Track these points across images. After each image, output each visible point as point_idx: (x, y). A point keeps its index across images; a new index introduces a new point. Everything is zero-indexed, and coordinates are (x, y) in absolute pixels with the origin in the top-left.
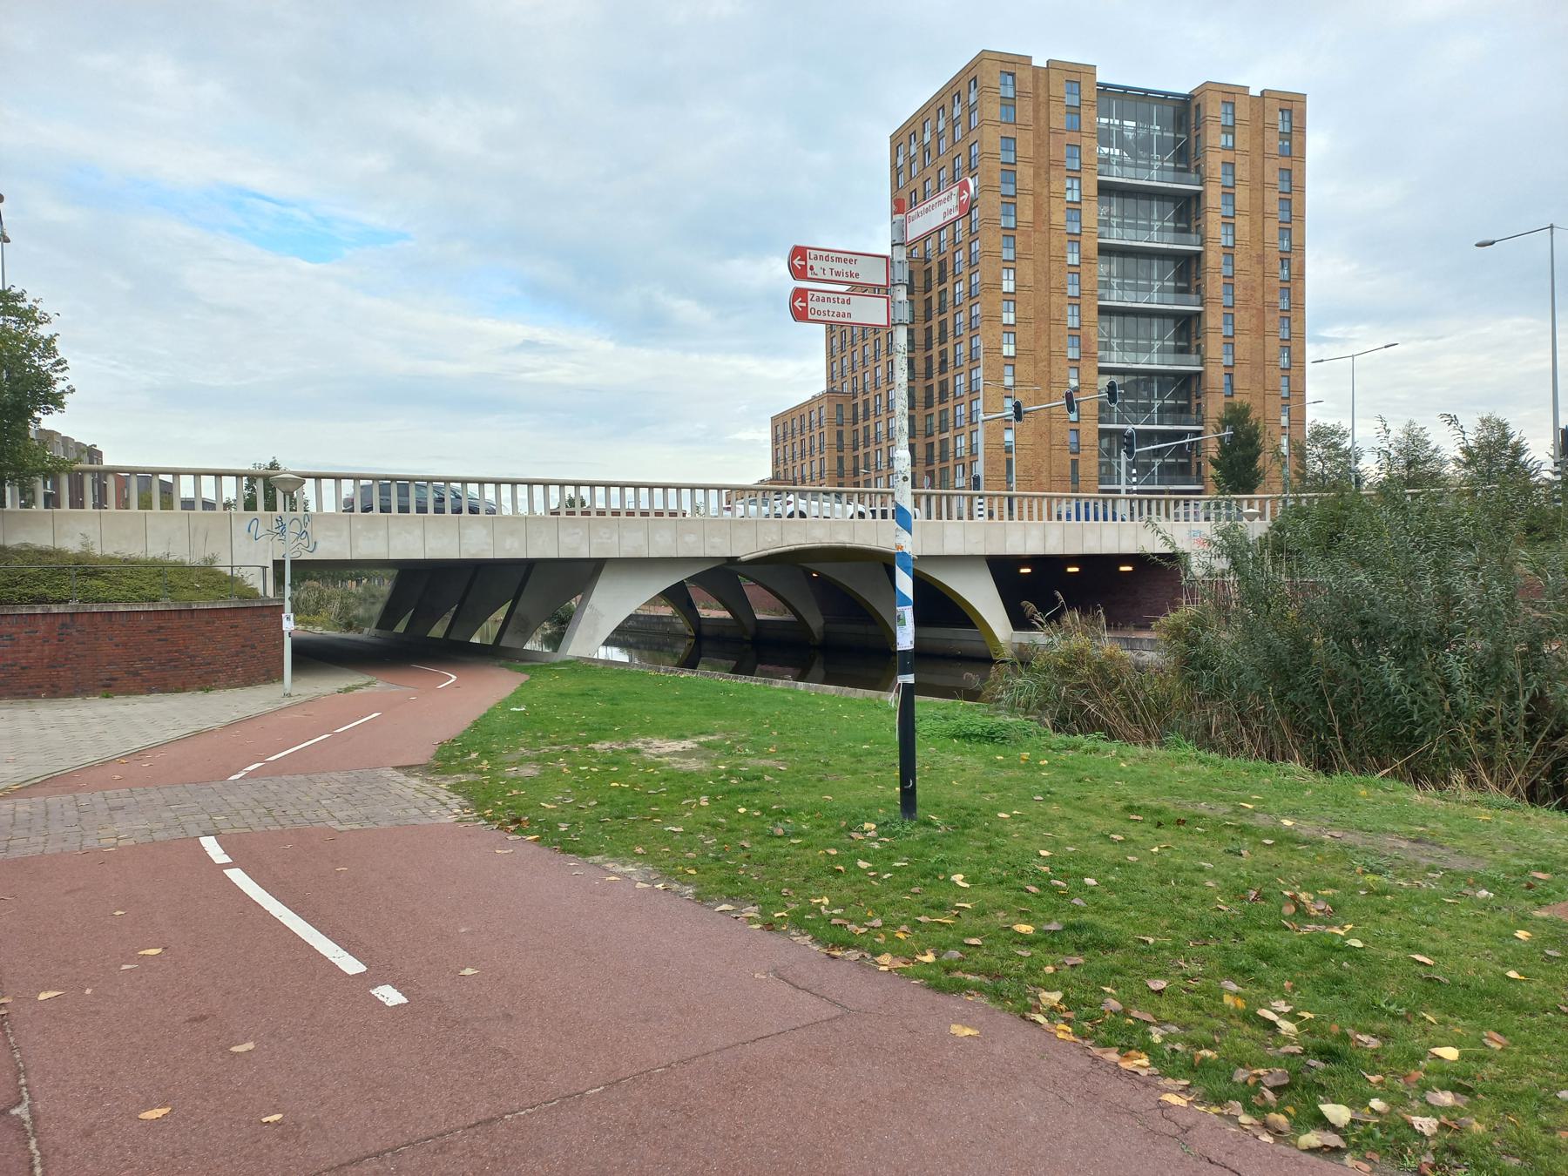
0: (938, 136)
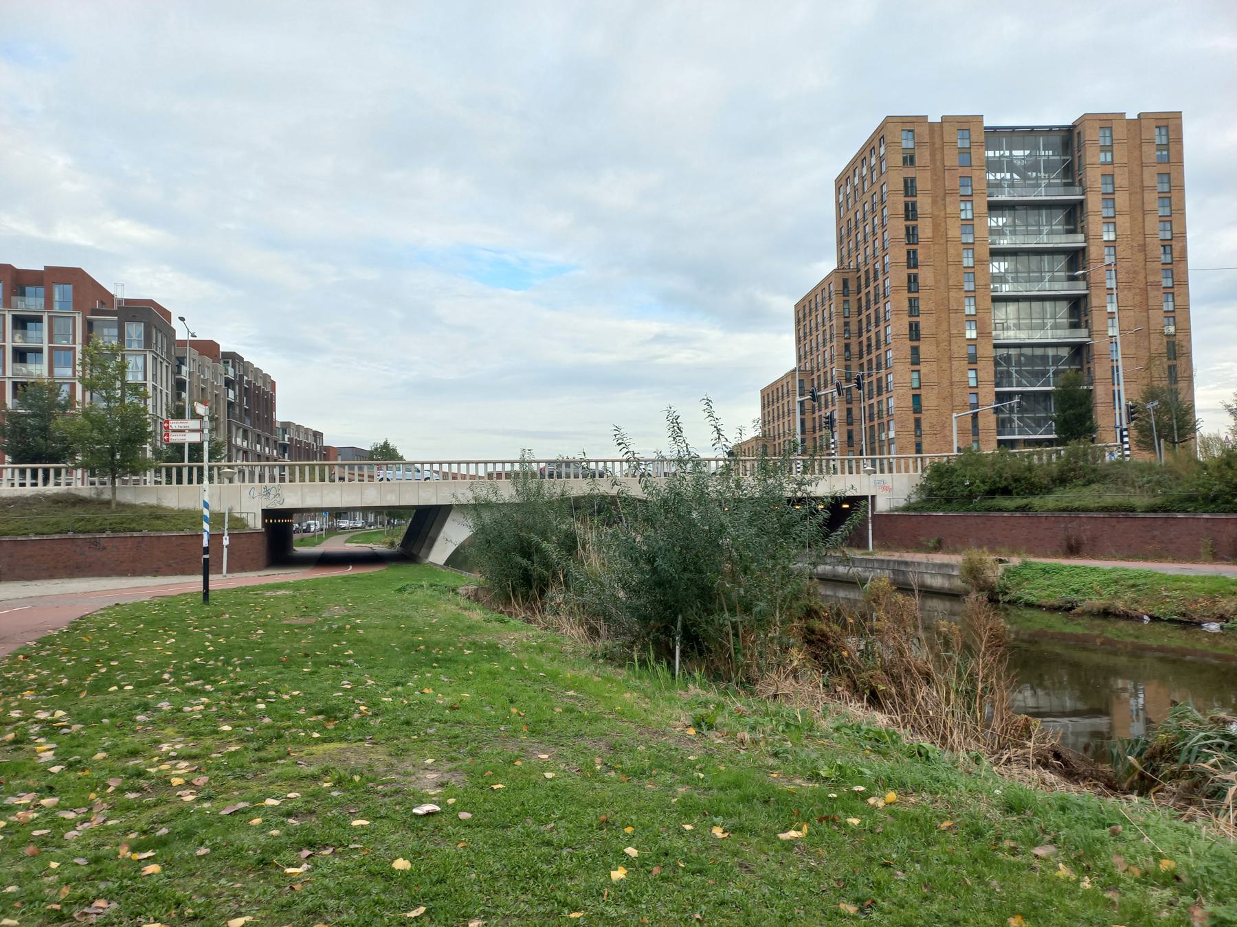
0: (862, 179)
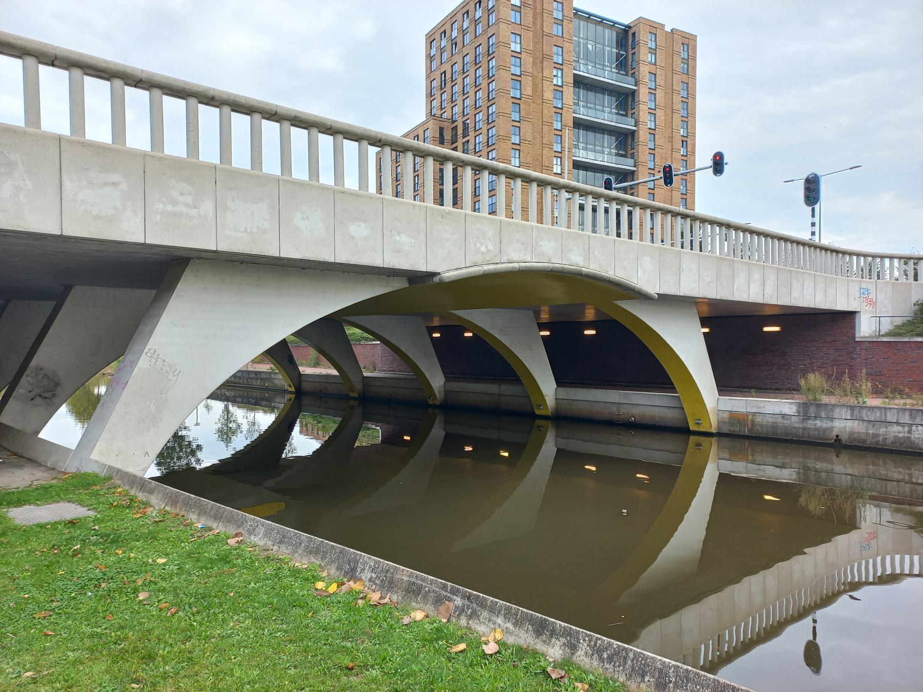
0: (463, 32)
